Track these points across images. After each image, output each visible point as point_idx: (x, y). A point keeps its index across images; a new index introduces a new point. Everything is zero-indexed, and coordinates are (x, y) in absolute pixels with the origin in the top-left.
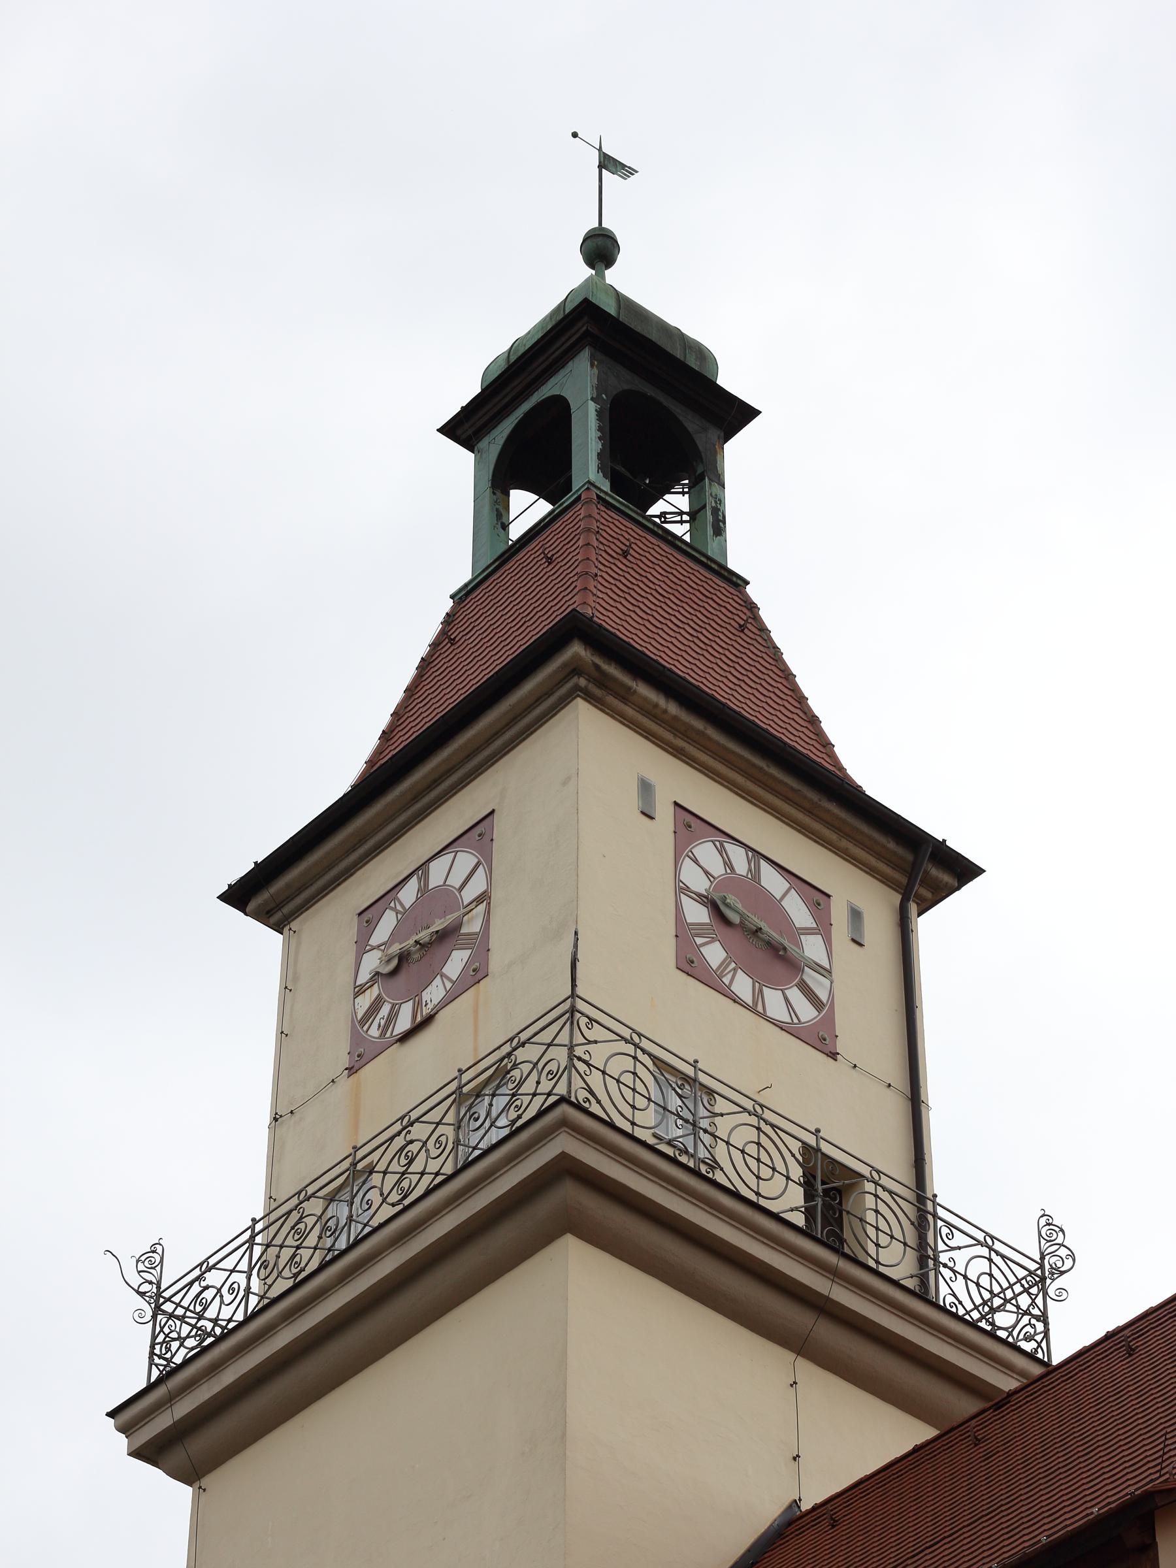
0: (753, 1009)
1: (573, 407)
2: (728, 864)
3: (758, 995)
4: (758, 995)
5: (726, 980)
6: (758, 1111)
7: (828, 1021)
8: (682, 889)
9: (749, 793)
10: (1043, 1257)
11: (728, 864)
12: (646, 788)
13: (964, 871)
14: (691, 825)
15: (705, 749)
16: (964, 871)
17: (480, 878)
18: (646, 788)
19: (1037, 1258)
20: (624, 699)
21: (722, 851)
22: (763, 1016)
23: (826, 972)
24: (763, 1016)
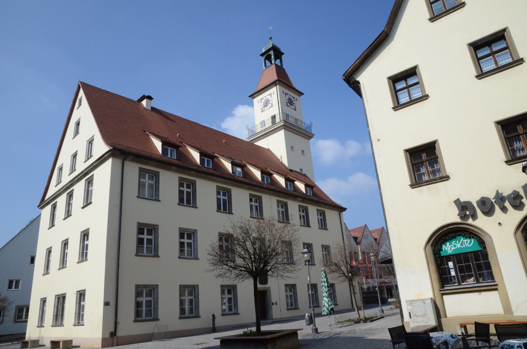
14: (286, 94)
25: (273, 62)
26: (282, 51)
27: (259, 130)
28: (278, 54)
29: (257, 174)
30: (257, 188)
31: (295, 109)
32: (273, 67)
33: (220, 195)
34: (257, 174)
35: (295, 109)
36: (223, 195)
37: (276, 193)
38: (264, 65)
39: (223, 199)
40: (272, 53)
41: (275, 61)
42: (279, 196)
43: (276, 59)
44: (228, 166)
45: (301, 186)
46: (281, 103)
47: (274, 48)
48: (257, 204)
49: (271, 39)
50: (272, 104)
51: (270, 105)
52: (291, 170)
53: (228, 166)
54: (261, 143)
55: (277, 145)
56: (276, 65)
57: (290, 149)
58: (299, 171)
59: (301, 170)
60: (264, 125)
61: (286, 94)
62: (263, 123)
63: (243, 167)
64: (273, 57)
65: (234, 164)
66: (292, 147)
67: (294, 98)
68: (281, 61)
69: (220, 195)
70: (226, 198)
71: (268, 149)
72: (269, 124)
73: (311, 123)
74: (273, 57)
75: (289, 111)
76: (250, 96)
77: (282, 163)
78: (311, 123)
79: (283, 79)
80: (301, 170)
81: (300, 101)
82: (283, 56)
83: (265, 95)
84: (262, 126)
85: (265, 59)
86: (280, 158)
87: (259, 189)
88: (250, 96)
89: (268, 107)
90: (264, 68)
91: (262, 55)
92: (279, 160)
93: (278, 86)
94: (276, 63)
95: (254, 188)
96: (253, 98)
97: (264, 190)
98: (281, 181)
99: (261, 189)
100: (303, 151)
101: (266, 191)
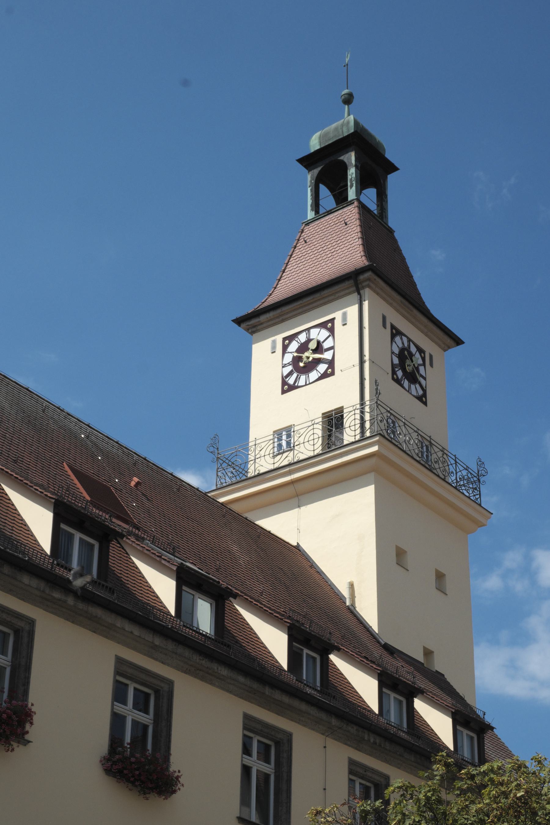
0: (408, 391)
1: (347, 163)
2: (403, 343)
3: (409, 387)
4: (409, 387)
5: (402, 382)
6: (443, 450)
7: (425, 395)
8: (393, 353)
9: (299, 313)
10: (478, 472)
11: (403, 343)
12: (384, 318)
13: (463, 343)
14: (395, 332)
15: (288, 313)
16: (463, 343)
17: (414, 392)
18: (384, 318)
19: (477, 472)
20: (262, 324)
21: (401, 339)
22: (411, 393)
23: (425, 379)
24: (411, 393)
25: (352, 194)
26: (388, 155)
27: (264, 464)
28: (377, 169)
29: (275, 642)
30: (278, 695)
31: (422, 399)
32: (351, 213)
33: (125, 703)
34: (275, 642)
35: (422, 399)
36: (136, 706)
37: (353, 729)
38: (310, 202)
39: (135, 723)
40: (351, 158)
41: (359, 192)
42: (357, 744)
43: (364, 183)
44: (164, 588)
45: (440, 724)
46: (372, 362)
47: (359, 140)
48: (269, 769)
49: (348, 100)
50: (331, 363)
51: (322, 368)
52: (389, 649)
53: (164, 588)
54: (281, 525)
55: (340, 539)
56: (363, 209)
57: (393, 557)
58: (420, 657)
59: (428, 653)
60: (290, 447)
61: (395, 332)
62: (284, 437)
63: (220, 598)
64: (352, 172)
65: (186, 580)
66: (400, 554)
67: (421, 351)
68: (382, 196)
69: (125, 703)
70: (147, 719)
71: (298, 547)
72: (309, 443)
73: (480, 463)
74: (352, 172)
75: (401, 399)
76: (239, 321)
77: (352, 611)
78: (480, 463)
79: (384, 272)
80: (428, 653)
81: (443, 371)
82: (392, 179)
83: (308, 328)
84: (280, 451)
85: (318, 181)
86: (345, 592)
87: (286, 699)
88: (239, 321)
89: (314, 375)
90: (311, 215)
91: (308, 161)
92: (341, 598)
93: (367, 292)
94: (363, 198)
95: (267, 691)
96: (253, 330)
97: (303, 707)
98: (366, 687)
99: (296, 703)
100: (440, 576)
101: (313, 711)
